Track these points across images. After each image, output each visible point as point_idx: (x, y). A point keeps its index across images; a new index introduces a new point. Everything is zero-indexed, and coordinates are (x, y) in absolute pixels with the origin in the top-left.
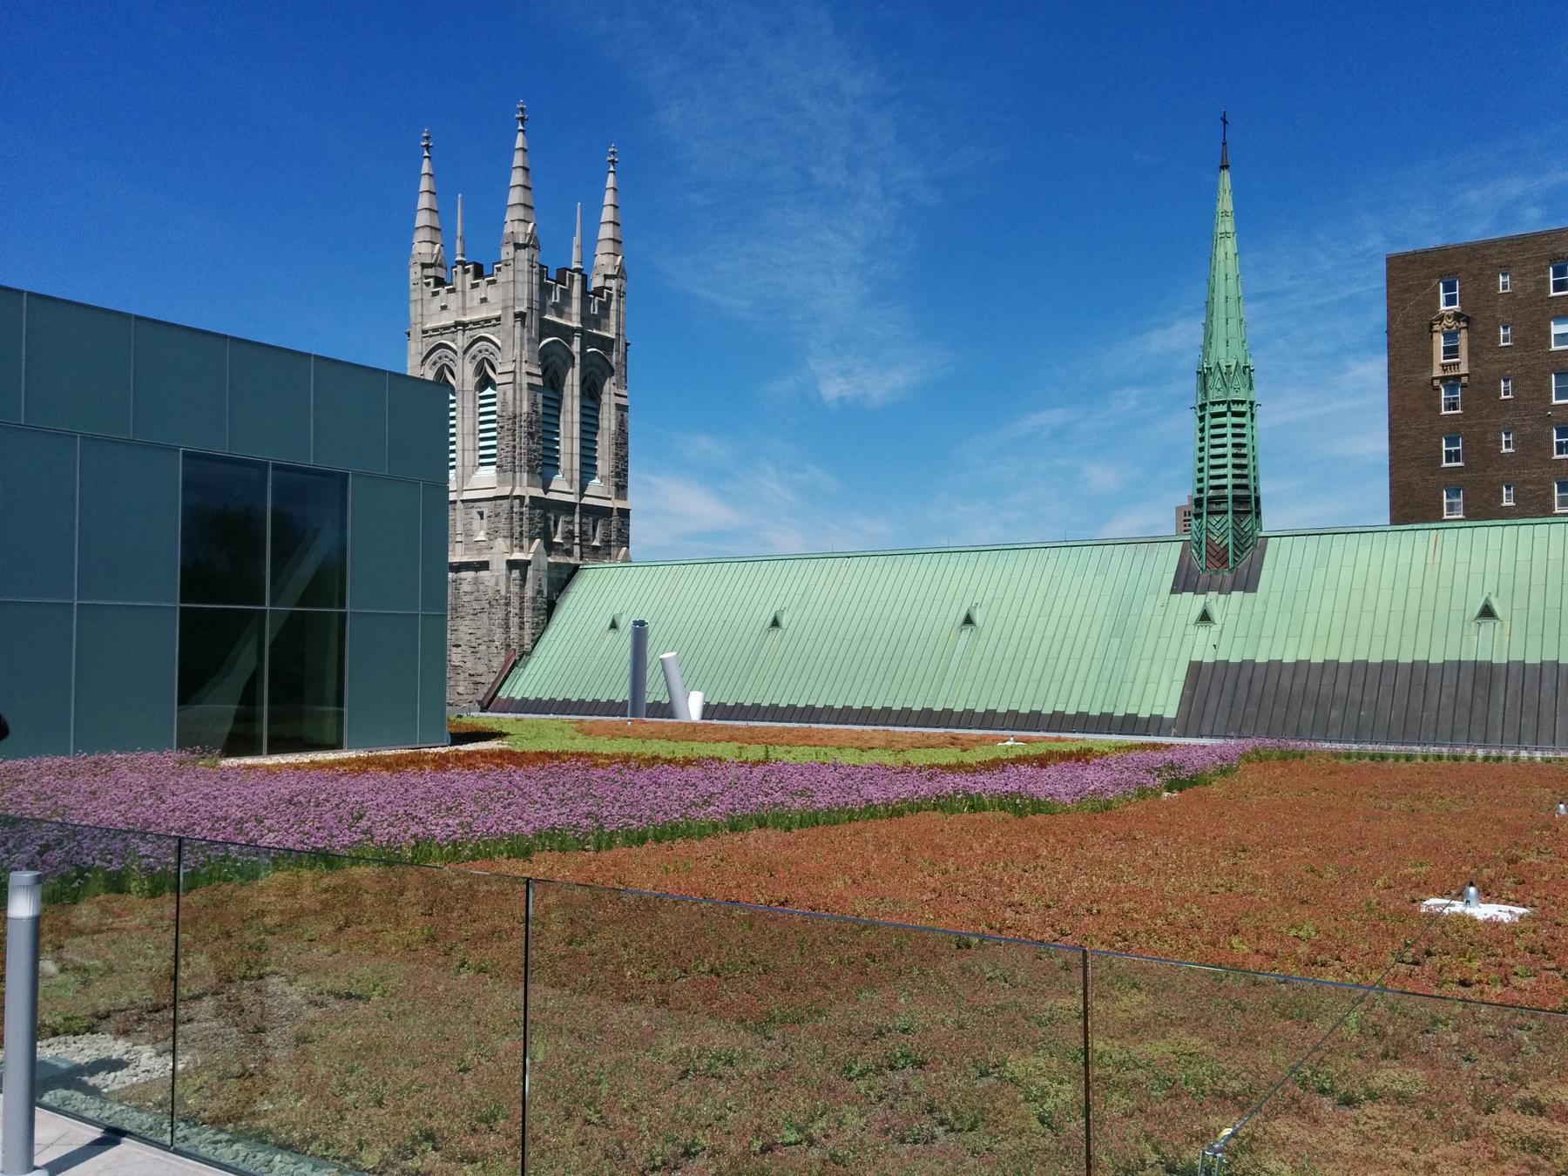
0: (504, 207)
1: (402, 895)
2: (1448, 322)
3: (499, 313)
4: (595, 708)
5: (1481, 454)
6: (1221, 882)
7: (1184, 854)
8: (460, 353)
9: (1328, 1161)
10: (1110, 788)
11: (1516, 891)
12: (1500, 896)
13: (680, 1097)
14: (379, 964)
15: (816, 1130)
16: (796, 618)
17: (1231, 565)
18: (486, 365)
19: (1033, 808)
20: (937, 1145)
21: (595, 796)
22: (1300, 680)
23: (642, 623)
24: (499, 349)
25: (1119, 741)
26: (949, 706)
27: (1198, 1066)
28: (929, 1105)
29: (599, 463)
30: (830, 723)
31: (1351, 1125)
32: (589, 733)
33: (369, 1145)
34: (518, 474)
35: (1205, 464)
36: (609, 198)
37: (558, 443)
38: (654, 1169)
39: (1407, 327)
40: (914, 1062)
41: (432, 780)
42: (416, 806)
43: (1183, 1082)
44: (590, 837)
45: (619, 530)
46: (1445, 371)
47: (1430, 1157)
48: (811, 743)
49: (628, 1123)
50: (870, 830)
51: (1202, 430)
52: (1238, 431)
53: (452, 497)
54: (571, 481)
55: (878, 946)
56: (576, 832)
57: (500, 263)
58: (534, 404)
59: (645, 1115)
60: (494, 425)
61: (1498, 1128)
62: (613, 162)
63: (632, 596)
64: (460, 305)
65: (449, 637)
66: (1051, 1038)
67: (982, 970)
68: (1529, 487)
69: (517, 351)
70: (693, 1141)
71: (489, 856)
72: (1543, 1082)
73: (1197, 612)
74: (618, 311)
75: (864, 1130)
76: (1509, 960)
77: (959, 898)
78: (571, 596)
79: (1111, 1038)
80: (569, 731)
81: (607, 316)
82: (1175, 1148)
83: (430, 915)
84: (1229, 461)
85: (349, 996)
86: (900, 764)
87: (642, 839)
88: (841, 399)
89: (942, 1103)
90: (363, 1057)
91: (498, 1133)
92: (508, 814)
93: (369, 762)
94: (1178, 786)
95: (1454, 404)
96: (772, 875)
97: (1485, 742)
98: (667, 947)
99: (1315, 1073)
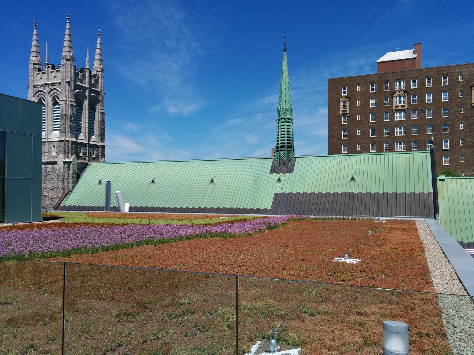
0: (62, 47)
1: (24, 270)
2: (344, 99)
3: (60, 81)
4: (93, 208)
5: (352, 135)
6: (281, 255)
7: (271, 248)
8: (47, 93)
9: (306, 332)
10: (251, 230)
11: (358, 255)
12: (353, 256)
13: (117, 329)
14: (16, 292)
15: (160, 335)
16: (160, 180)
17: (286, 165)
19: (229, 236)
20: (197, 336)
21: (92, 236)
22: (304, 198)
23: (109, 182)
24: (61, 93)
25: (255, 216)
26: (206, 207)
27: (272, 308)
28: (195, 325)
29: (95, 131)
30: (170, 212)
31: (312, 321)
32: (91, 216)
33: (11, 350)
34: (67, 134)
35: (279, 136)
36: (98, 46)
37: (81, 124)
38: (108, 351)
39: (333, 100)
40: (191, 312)
41: (36, 233)
42: (30, 241)
43: (268, 312)
44: (90, 249)
45: (102, 152)
46: (343, 112)
47: (332, 329)
48: (164, 218)
49: (100, 338)
50: (180, 244)
51: (278, 127)
52: (288, 127)
53: (43, 140)
54: (86, 136)
55: (182, 279)
56: (85, 248)
57: (61, 65)
58: (73, 111)
59: (106, 334)
60: (59, 117)
61: (350, 320)
62: (99, 35)
63: (106, 173)
64: (47, 78)
65: (43, 186)
66: (231, 302)
67: (212, 284)
68: (364, 145)
69: (67, 94)
70: (121, 341)
71: (55, 256)
72: (362, 307)
73: (277, 179)
74: (101, 82)
75: (175, 334)
76: (355, 274)
77: (207, 263)
78: (85, 173)
79: (248, 301)
80: (84, 216)
81: (98, 84)
82: (265, 331)
83: (34, 276)
84: (286, 136)
85: (5, 303)
86: (191, 224)
87: (108, 249)
88: (174, 113)
89: (199, 324)
90: (9, 323)
91: (56, 344)
92: (62, 243)
93: (13, 227)
94: (271, 228)
95: (345, 121)
96: (149, 259)
97: (352, 215)
98: (115, 282)
99: (303, 307)
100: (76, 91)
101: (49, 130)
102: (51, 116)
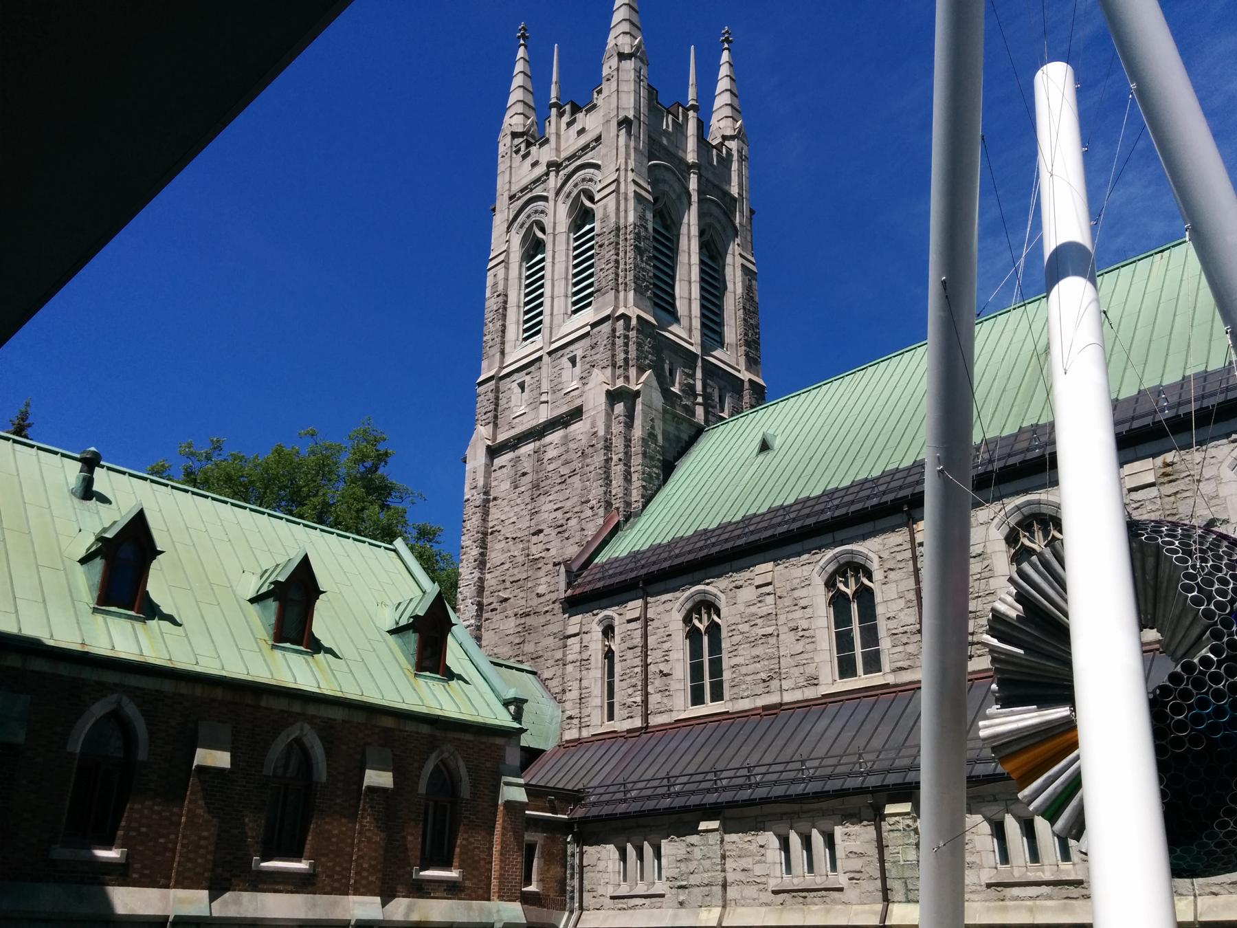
18: (583, 197)
34: (622, 294)
58: (642, 217)
69: (622, 160)
100: (653, 162)
101: (555, 313)
102: (564, 265)
